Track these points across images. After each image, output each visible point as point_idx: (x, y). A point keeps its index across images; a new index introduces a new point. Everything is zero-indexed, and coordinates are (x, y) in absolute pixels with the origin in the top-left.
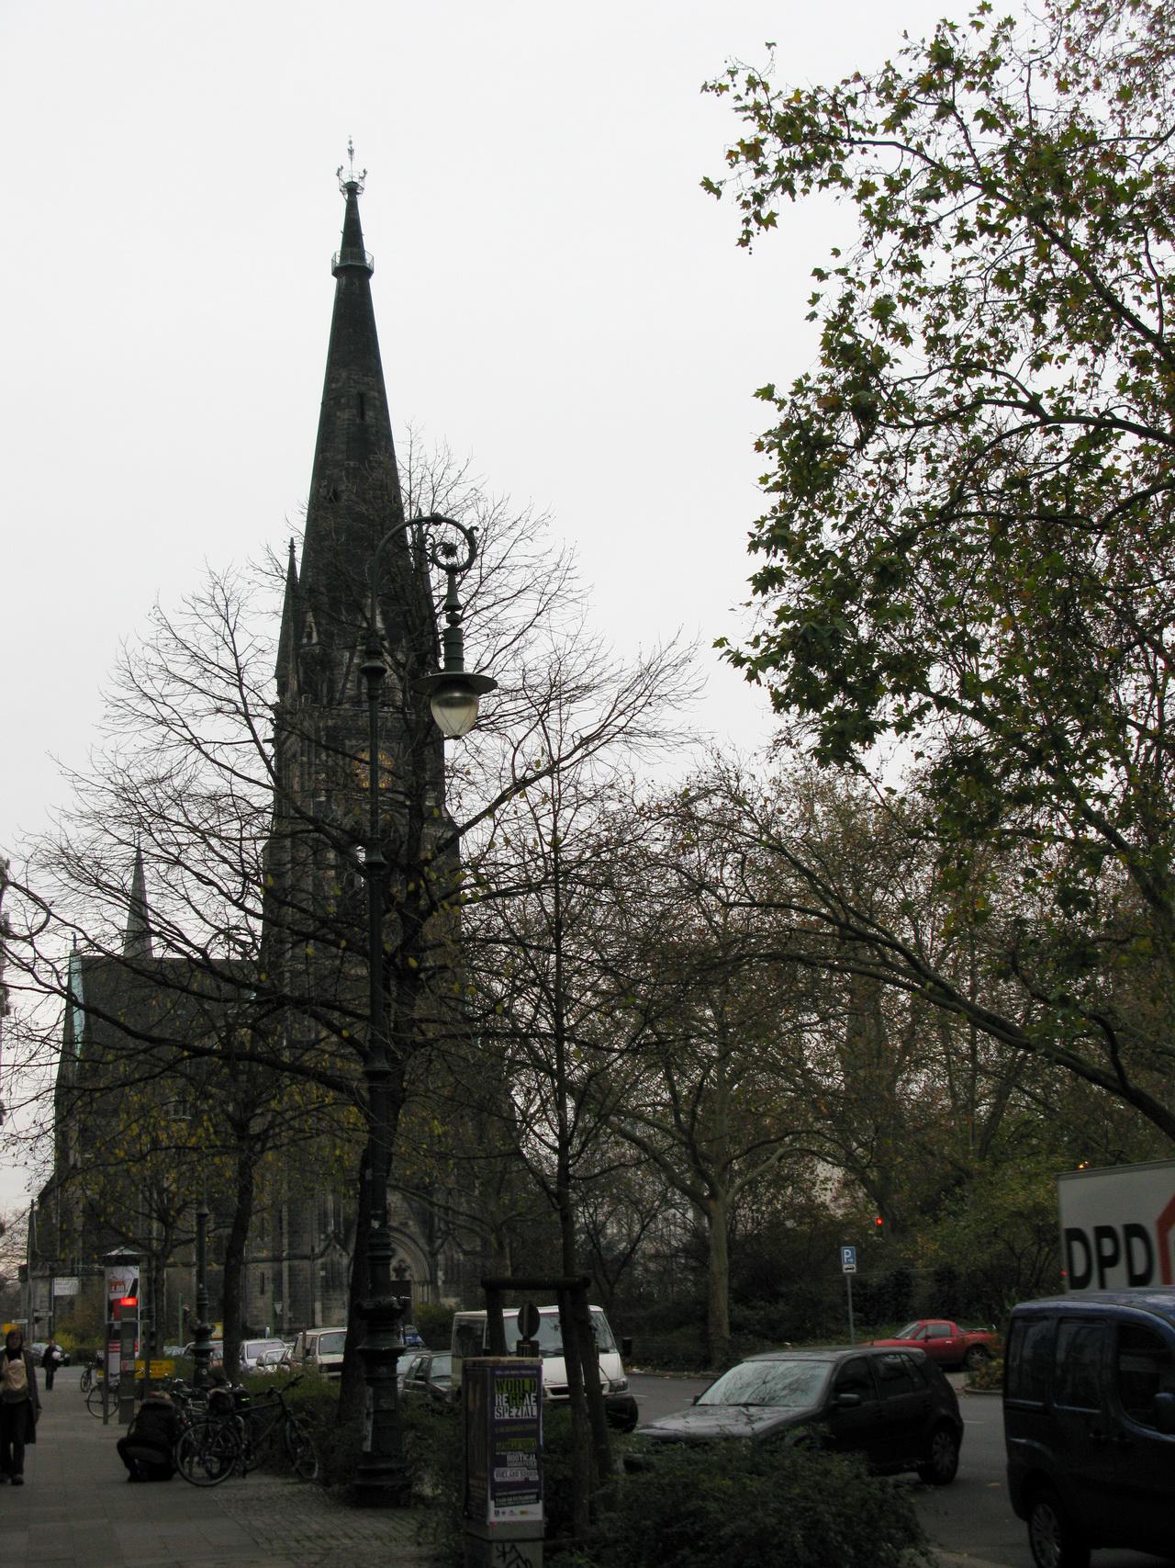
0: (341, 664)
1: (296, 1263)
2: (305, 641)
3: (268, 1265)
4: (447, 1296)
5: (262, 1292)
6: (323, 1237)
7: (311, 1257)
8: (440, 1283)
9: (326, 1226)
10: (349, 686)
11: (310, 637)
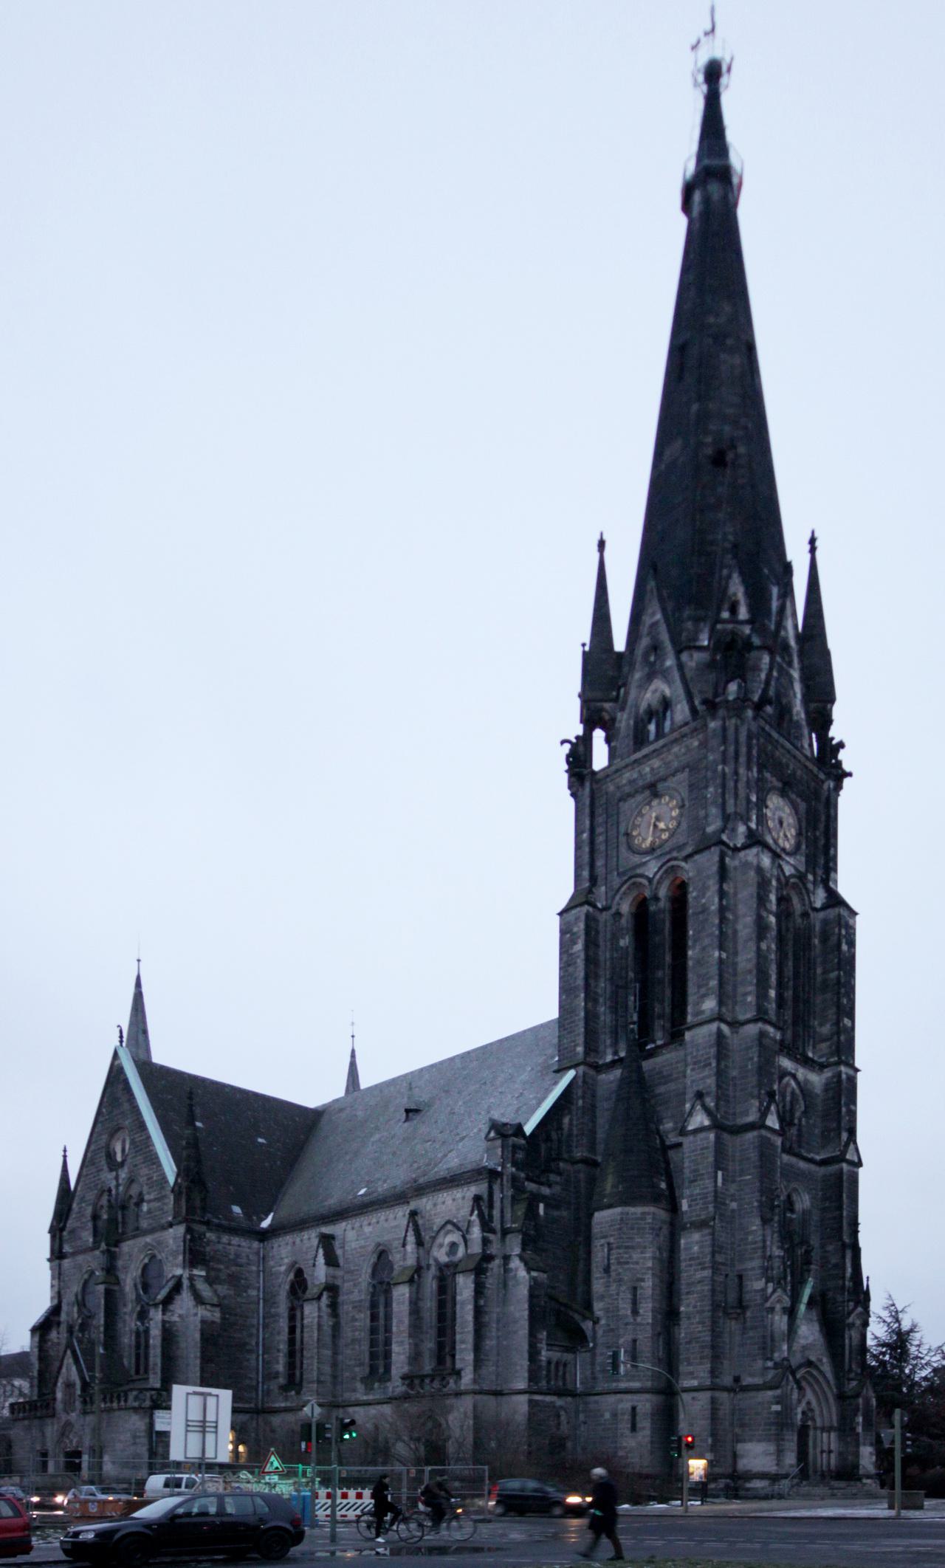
0: (757, 669)
1: (717, 1394)
2: (725, 615)
3: (648, 1396)
4: (864, 1445)
6: (770, 1364)
7: (737, 1387)
8: (860, 1429)
9: (772, 1352)
11: (734, 609)
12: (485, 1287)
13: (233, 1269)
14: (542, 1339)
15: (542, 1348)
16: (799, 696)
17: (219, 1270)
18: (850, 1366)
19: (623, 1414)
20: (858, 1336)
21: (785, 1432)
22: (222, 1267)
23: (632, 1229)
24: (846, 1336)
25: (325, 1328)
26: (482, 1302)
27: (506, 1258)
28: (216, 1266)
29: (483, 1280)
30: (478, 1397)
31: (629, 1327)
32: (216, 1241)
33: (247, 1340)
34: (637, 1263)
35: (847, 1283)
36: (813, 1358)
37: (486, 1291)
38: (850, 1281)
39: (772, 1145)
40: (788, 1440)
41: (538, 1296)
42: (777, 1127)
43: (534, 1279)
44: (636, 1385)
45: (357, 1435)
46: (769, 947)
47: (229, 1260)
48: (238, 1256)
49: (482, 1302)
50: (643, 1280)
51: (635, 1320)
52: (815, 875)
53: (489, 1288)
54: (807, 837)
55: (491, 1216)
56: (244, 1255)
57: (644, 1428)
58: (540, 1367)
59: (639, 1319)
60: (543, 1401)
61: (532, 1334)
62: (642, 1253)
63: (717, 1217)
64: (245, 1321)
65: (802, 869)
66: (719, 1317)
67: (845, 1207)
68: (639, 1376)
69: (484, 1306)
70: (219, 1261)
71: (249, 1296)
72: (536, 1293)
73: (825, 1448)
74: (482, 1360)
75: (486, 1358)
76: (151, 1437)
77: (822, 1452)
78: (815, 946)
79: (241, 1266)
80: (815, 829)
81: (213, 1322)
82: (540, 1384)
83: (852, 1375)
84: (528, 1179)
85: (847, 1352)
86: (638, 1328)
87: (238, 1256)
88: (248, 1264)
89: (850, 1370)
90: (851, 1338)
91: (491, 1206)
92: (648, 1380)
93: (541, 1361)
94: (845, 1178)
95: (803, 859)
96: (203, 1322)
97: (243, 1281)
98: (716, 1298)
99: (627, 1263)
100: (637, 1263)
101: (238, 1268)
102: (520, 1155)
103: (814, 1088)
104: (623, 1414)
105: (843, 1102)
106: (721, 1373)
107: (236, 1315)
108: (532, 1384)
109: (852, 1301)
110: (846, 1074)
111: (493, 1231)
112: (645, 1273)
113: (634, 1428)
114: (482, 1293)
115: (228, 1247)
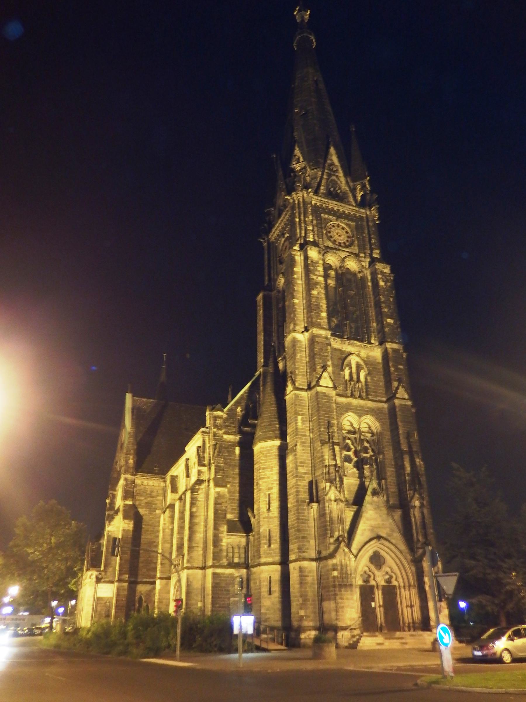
5: (270, 593)
10: (322, 188)
12: (197, 500)
13: (149, 499)
14: (223, 531)
15: (224, 537)
16: (344, 182)
17: (141, 500)
18: (417, 538)
19: (264, 581)
20: (420, 515)
21: (343, 592)
22: (143, 498)
23: (266, 456)
24: (412, 515)
25: (167, 530)
26: (194, 510)
27: (209, 481)
28: (139, 498)
29: (195, 496)
30: (190, 571)
31: (266, 519)
32: (141, 484)
33: (154, 540)
34: (268, 478)
35: (407, 478)
36: (384, 535)
37: (197, 502)
38: (408, 476)
39: (329, 397)
40: (347, 599)
41: (220, 504)
42: (331, 385)
43: (218, 493)
44: (270, 560)
45: (468, 606)
46: (319, 293)
47: (147, 494)
48: (152, 492)
49: (194, 510)
50: (271, 488)
51: (268, 515)
52: (364, 253)
53: (199, 501)
54: (358, 238)
55: (204, 457)
56: (155, 490)
57: (275, 591)
58: (221, 550)
59: (271, 514)
60: (223, 574)
61: (216, 528)
62: (271, 471)
63: (298, 444)
64: (154, 529)
65: (357, 252)
66: (304, 509)
67: (400, 427)
68: (271, 553)
69: (196, 512)
70: (141, 496)
71: (155, 514)
72: (219, 501)
73: (409, 604)
74: (194, 547)
75: (196, 545)
76: (94, 598)
77: (407, 606)
78: (368, 286)
79: (153, 497)
80: (363, 233)
81: (128, 530)
82: (221, 562)
83: (419, 545)
84: (225, 433)
85: (414, 527)
86: (270, 520)
87: (152, 492)
88: (158, 496)
89: (418, 540)
90: (415, 517)
91: (204, 452)
92: (276, 556)
93: (222, 546)
94: (397, 410)
95: (356, 248)
96: (124, 530)
97: (153, 506)
98: (300, 496)
99: (264, 478)
100: (268, 478)
101: (151, 499)
102: (219, 422)
103: (376, 359)
104: (264, 581)
105: (390, 365)
106: (307, 549)
107: (148, 525)
108: (215, 561)
109: (411, 490)
110: (392, 348)
111: (204, 465)
112: (272, 484)
113: (270, 593)
114: (195, 504)
115: (147, 487)
